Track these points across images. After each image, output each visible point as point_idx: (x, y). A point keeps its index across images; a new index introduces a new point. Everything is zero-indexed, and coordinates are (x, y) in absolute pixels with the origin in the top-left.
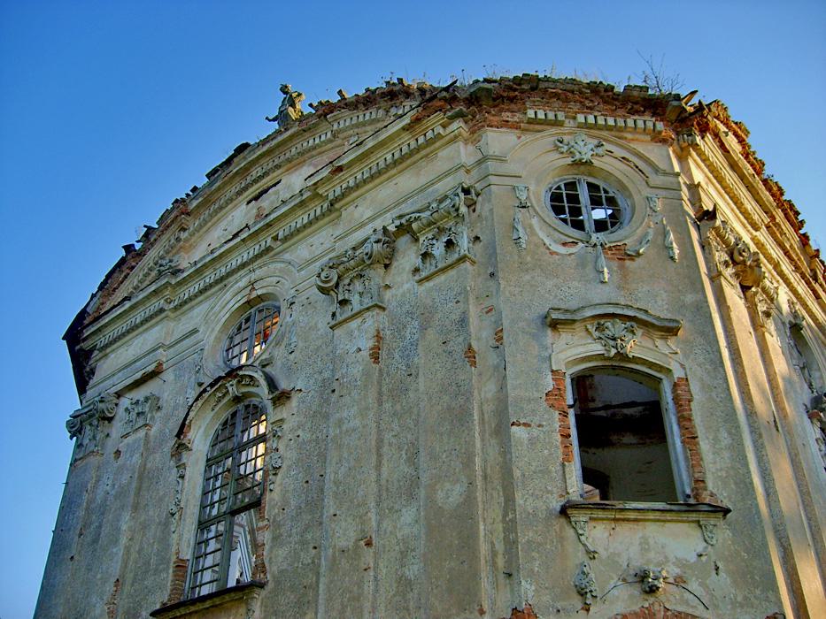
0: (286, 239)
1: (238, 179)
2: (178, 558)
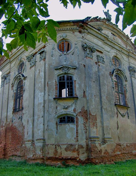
0: (122, 53)
1: (112, 28)
2: (86, 98)
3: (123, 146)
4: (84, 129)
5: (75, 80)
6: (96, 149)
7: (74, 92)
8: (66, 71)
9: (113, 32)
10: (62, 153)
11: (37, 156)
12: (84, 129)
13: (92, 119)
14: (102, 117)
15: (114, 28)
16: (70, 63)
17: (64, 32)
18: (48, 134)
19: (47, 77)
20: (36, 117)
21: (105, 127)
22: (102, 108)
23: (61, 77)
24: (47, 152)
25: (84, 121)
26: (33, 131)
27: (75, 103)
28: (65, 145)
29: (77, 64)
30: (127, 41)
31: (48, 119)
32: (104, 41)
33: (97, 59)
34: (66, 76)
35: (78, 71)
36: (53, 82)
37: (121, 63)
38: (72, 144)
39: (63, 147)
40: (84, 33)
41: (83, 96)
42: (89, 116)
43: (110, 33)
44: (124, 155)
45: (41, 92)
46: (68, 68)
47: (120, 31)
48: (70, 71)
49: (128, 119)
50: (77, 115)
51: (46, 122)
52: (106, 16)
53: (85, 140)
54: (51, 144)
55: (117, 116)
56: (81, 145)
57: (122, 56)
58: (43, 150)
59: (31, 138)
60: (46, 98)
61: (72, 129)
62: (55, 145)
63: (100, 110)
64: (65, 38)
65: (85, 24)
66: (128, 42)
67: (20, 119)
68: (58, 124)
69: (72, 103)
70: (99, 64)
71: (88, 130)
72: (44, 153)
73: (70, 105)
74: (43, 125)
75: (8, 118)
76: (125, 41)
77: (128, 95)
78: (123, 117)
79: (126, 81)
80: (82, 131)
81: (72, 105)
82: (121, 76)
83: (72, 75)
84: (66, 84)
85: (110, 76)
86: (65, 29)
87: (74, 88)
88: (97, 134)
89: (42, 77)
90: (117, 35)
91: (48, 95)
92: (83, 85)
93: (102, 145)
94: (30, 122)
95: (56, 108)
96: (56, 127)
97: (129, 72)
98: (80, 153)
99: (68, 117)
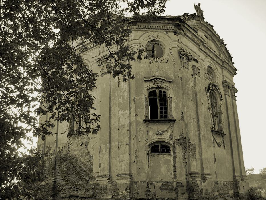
0: (217, 62)
1: (207, 29)
3: (220, 184)
4: (184, 162)
5: (170, 97)
6: (197, 188)
7: (169, 113)
8: (159, 84)
9: (207, 34)
10: (157, 194)
11: (119, 197)
12: (184, 161)
13: (191, 149)
14: (200, 146)
15: (209, 30)
16: (163, 74)
17: (154, 31)
18: (137, 168)
19: (133, 90)
20: (115, 144)
21: (204, 161)
22: (199, 134)
23: (151, 92)
24: (136, 192)
25: (183, 151)
26: (110, 163)
27: (171, 127)
28: (160, 182)
29: (172, 75)
30: (221, 46)
31: (137, 148)
32: (199, 46)
33: (192, 70)
34: (157, 91)
35: (174, 85)
36: (142, 99)
37: (215, 76)
38: (169, 182)
39: (157, 185)
40: (180, 34)
41: (181, 119)
42: (188, 145)
43: (204, 35)
44: (221, 196)
45: (124, 109)
46: (161, 80)
47: (214, 33)
48: (164, 84)
49: (224, 149)
50: (174, 144)
51: (133, 151)
52: (197, 11)
53: (185, 176)
54: (141, 181)
55: (213, 146)
56: (181, 183)
57: (216, 66)
58: (131, 189)
59: (106, 173)
60: (133, 119)
61: (167, 162)
62: (147, 182)
63: (198, 138)
64: (156, 39)
65: (182, 23)
66: (222, 49)
67: (83, 146)
68: (149, 154)
69: (168, 127)
70: (196, 76)
71: (187, 162)
72: (131, 193)
73: (165, 129)
74: (129, 155)
75: (58, 143)
76: (218, 46)
77: (223, 118)
78: (219, 147)
79: (221, 100)
80: (181, 165)
81: (167, 131)
82: (215, 93)
83: (165, 90)
84: (158, 101)
85: (205, 93)
86: (156, 27)
87: (169, 106)
88: (197, 170)
89: (124, 89)
90: (210, 38)
91: (136, 115)
92: (181, 104)
93: (203, 183)
94: (104, 151)
95: (147, 133)
96: (147, 158)
97: (223, 88)
98: (179, 192)
99: (162, 146)
